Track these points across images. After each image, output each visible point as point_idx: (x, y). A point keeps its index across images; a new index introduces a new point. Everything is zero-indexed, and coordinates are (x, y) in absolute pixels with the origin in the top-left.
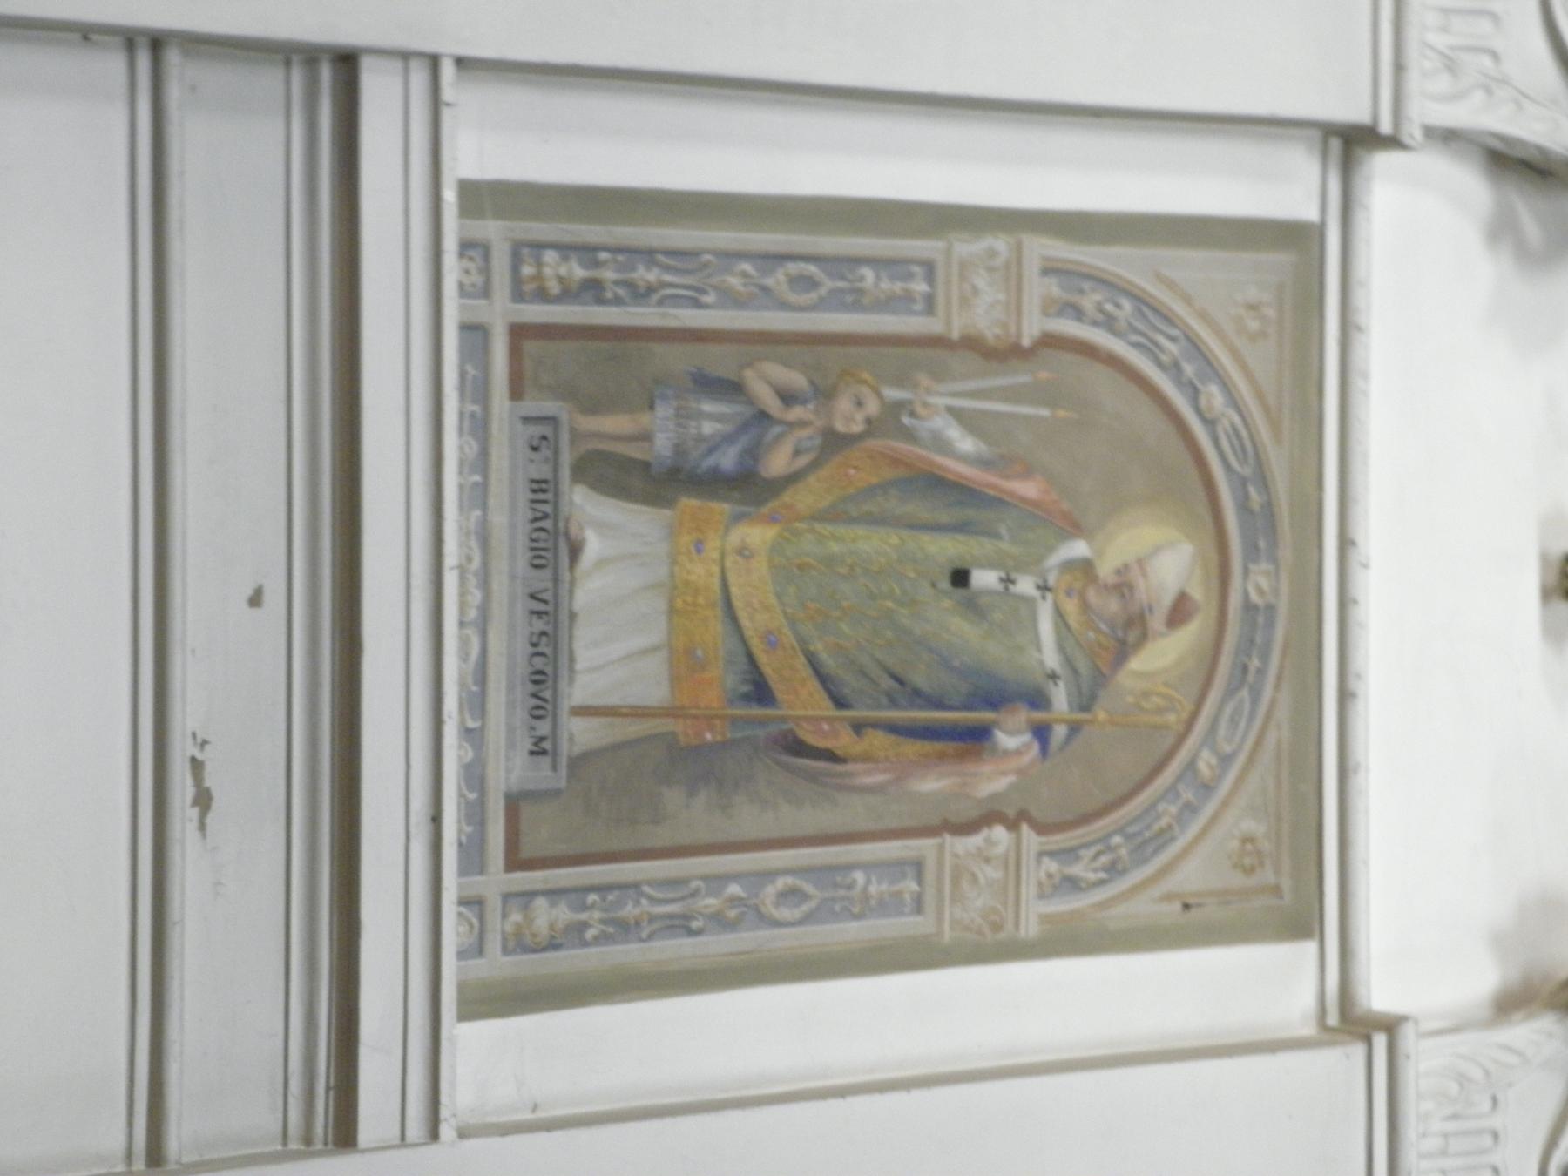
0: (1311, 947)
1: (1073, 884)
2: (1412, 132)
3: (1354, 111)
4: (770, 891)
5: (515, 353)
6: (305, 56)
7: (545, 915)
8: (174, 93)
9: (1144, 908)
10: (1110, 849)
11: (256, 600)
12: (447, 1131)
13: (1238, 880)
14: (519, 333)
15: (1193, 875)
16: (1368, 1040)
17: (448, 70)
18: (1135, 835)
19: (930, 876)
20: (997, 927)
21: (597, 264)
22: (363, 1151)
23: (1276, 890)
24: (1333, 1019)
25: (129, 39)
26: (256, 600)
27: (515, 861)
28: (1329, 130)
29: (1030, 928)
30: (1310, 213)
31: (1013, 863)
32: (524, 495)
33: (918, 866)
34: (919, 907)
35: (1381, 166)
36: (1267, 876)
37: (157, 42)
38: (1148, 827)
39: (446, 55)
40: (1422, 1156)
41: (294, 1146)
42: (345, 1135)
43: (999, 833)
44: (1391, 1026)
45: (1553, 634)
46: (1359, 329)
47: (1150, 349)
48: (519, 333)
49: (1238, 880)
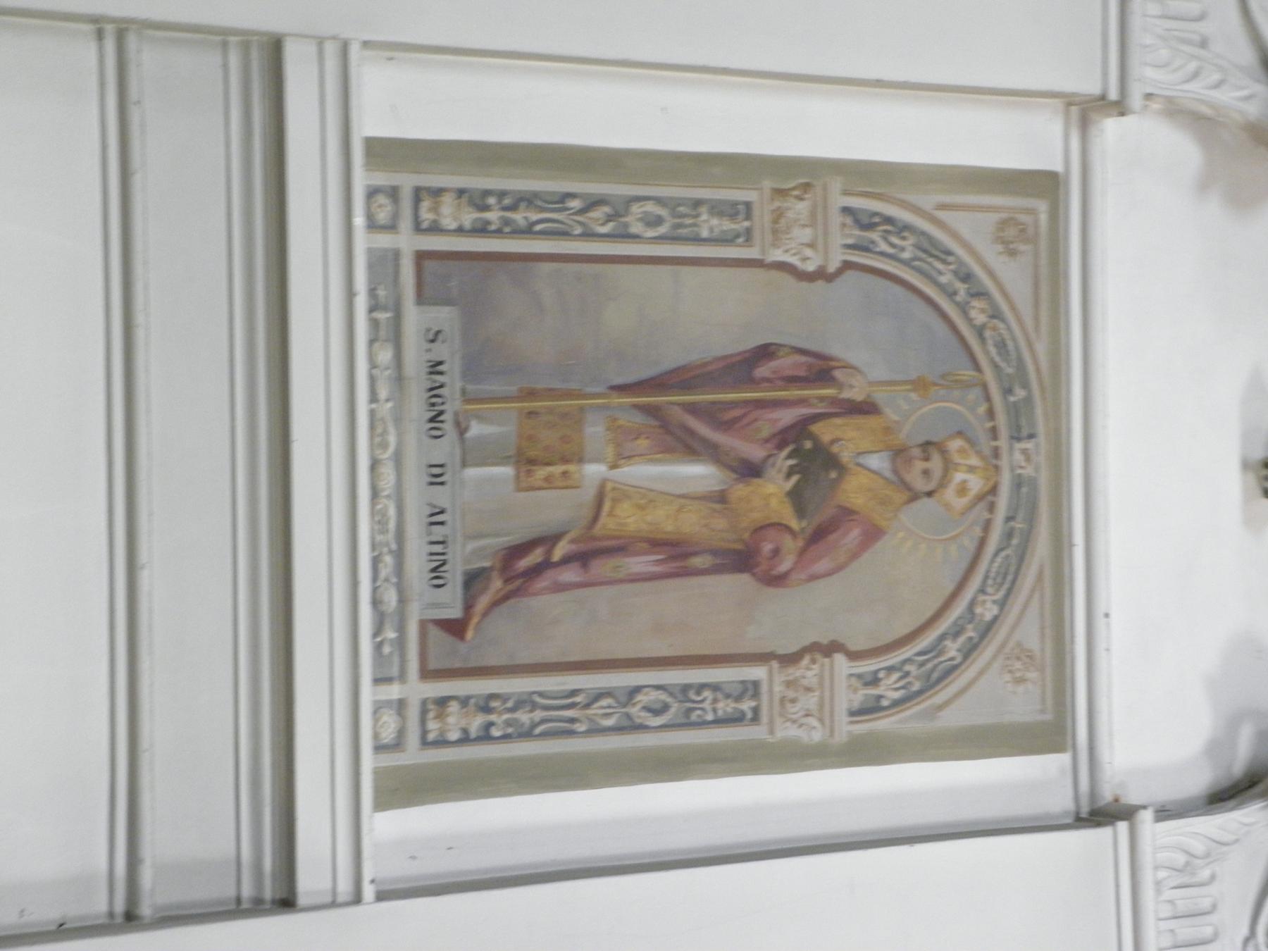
0: (1064, 759)
3: (1091, 87)
7: (455, 721)
10: (907, 674)
11: (413, 858)
14: (421, 257)
17: (355, 50)
19: (765, 698)
21: (486, 208)
25: (98, 24)
26: (413, 858)
30: (1058, 167)
34: (756, 719)
35: (1111, 129)
45: (1251, 522)
46: (1074, 545)
48: (421, 257)
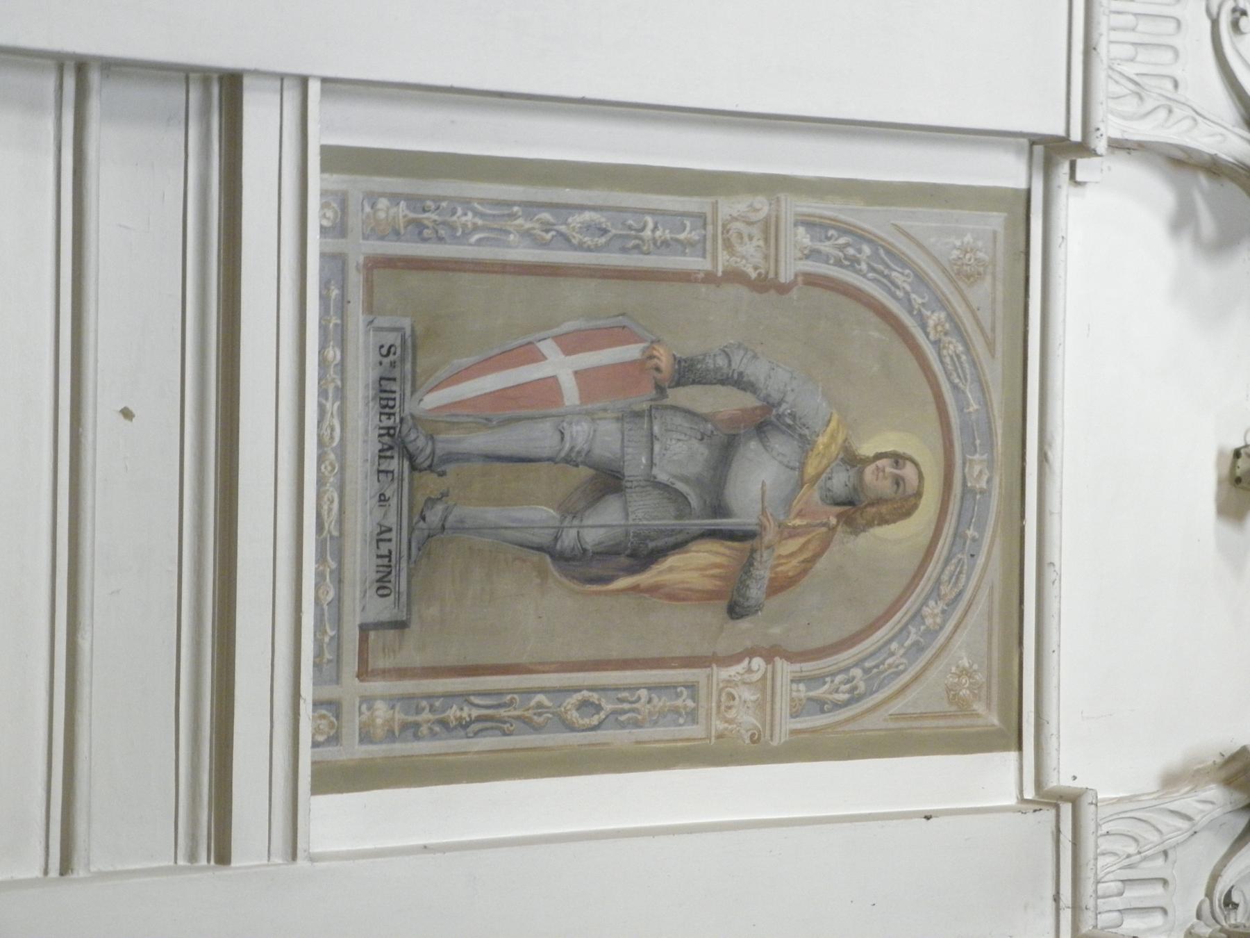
1: (820, 706)
2: (1101, 145)
3: (1055, 127)
6: (205, 76)
8: (95, 106)
16: (1057, 807)
17: (314, 88)
18: (870, 669)
19: (703, 693)
24: (1029, 794)
27: (364, 673)
28: (1035, 140)
29: (781, 737)
31: (766, 686)
32: (374, 357)
33: (692, 687)
37: (81, 66)
38: (883, 663)
39: (315, 77)
41: (181, 862)
42: (223, 856)
43: (758, 662)
44: (1074, 799)
47: (890, 286)
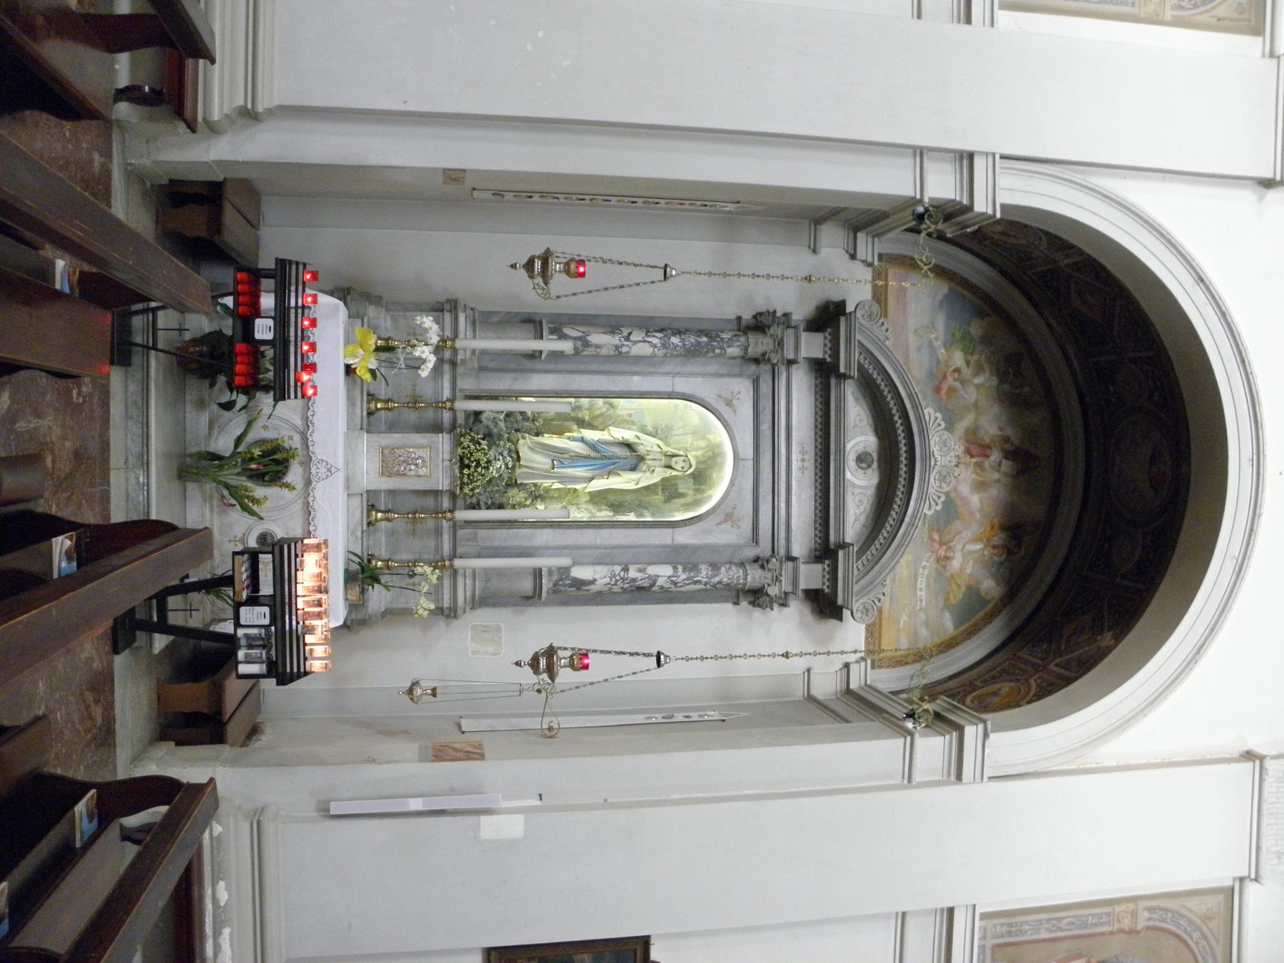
0: (1260, 39)
1: (1182, 8)
4: (1065, 922)
5: (993, 954)
9: (1204, 18)
12: (985, 778)
13: (1236, 15)
15: (1221, 11)
20: (1158, 15)
22: (965, 784)
23: (1249, 21)
29: (1168, 17)
36: (1246, 16)
40: (1269, 793)
49: (1236, 15)
